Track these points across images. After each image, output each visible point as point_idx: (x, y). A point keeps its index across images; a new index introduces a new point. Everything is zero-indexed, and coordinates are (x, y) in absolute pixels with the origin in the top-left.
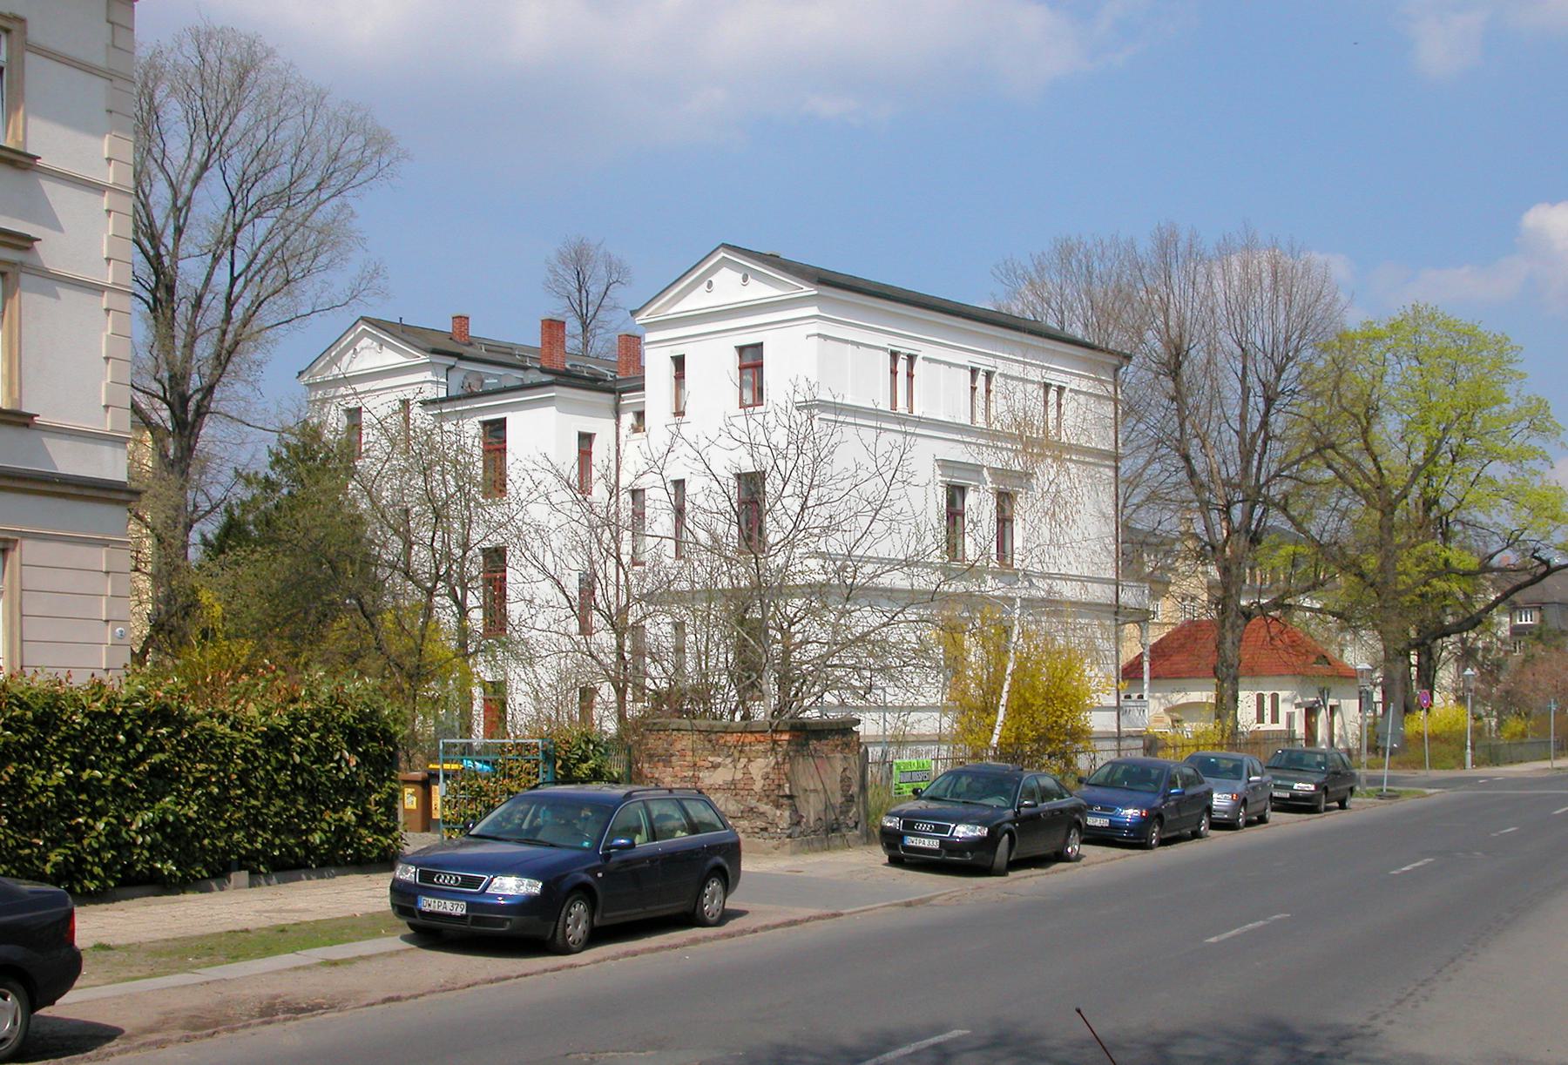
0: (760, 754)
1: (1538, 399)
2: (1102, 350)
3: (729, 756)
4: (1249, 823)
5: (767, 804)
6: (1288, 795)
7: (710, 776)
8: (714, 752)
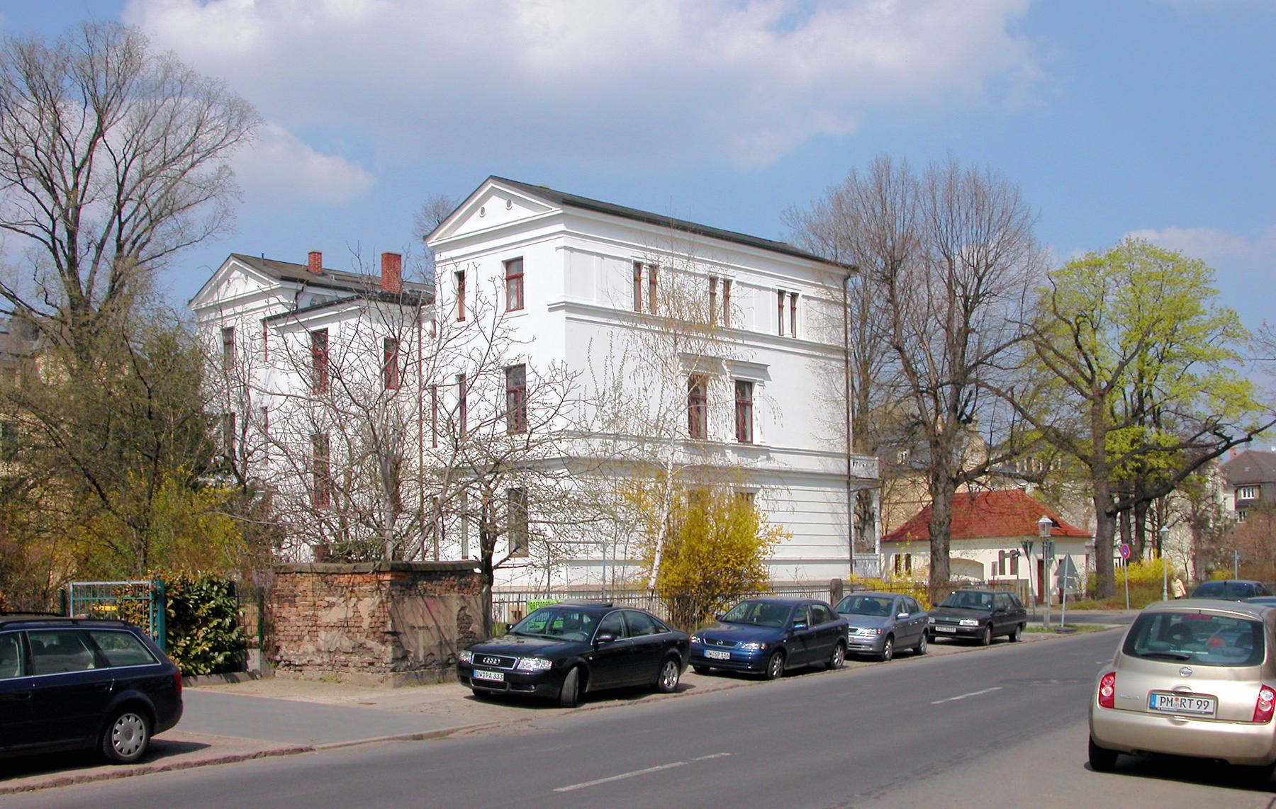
0: (367, 594)
1: (1228, 310)
2: (828, 262)
3: (343, 596)
4: (898, 655)
5: (373, 640)
6: (955, 631)
7: (327, 615)
8: (329, 594)
